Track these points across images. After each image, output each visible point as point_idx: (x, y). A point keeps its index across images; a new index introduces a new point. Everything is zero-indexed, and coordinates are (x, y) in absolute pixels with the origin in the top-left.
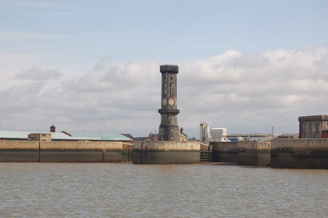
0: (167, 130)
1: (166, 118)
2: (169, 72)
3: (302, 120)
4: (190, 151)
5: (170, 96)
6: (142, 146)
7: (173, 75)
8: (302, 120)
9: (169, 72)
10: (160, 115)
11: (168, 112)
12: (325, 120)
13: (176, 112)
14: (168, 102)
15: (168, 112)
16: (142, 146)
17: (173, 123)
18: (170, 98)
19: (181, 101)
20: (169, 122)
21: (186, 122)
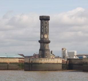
0: (43, 52)
1: (43, 45)
2: (44, 20)
4: (56, 64)
6: (29, 61)
7: (46, 22)
9: (44, 20)
10: (39, 44)
11: (44, 42)
14: (44, 36)
15: (44, 42)
16: (29, 61)
17: (47, 48)
19: (51, 36)
20: (44, 47)
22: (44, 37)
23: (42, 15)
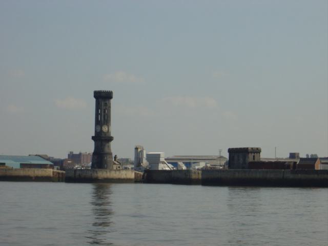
2: (103, 98)
3: (231, 151)
5: (104, 123)
8: (231, 151)
9: (103, 98)
10: (93, 142)
11: (102, 139)
12: (251, 153)
13: (93, 138)
14: (101, 128)
15: (102, 139)
17: (106, 150)
18: (104, 124)
19: (115, 128)
21: (120, 148)
22: (101, 131)
23: (98, 89)
